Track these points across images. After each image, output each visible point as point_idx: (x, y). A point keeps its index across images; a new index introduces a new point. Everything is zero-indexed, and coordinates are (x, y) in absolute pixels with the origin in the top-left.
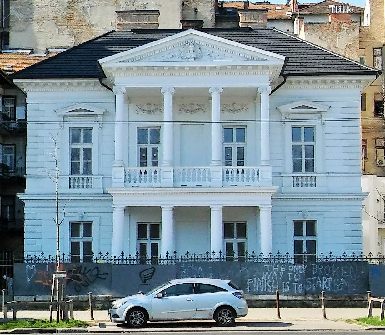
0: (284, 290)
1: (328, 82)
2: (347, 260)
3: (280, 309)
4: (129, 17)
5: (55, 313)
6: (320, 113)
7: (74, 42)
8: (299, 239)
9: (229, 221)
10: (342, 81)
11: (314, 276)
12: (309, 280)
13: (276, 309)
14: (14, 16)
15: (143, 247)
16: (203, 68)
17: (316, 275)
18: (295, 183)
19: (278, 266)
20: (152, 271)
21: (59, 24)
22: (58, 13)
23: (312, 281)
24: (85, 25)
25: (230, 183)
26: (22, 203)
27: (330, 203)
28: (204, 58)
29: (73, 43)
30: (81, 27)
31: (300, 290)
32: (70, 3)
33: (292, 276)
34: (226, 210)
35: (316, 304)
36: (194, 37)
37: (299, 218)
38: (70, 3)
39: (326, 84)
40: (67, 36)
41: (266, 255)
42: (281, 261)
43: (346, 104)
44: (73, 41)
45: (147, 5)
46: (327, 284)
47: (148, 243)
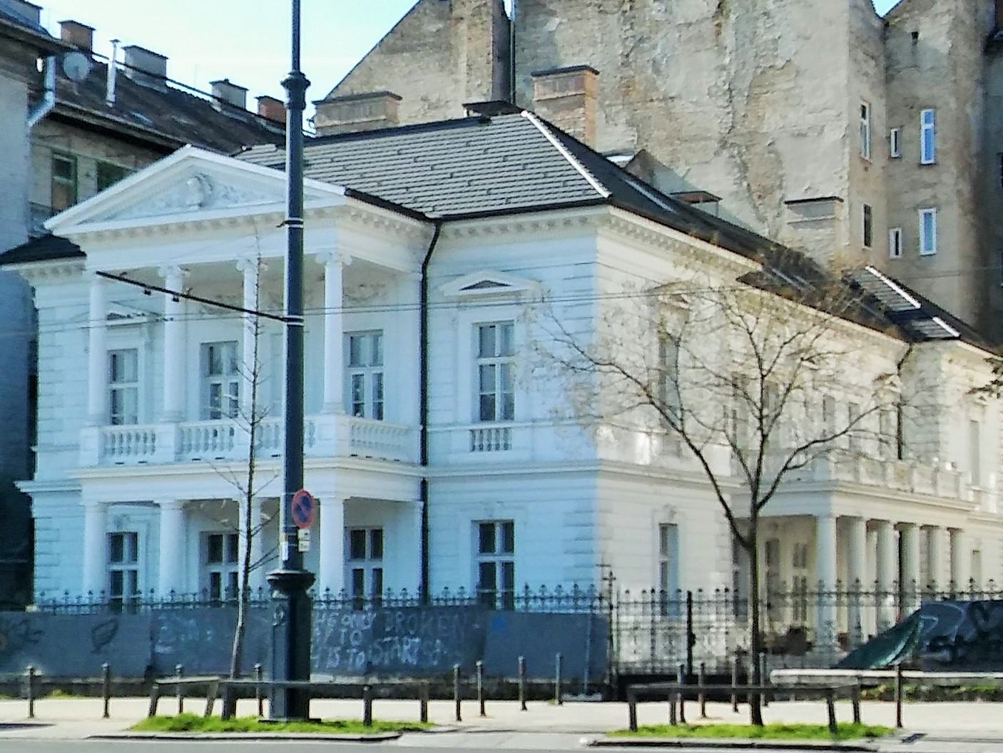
0: (330, 663)
1: (575, 222)
2: (450, 603)
3: (463, 703)
4: (335, 112)
5: (266, 703)
6: (517, 293)
7: (636, 139)
8: (488, 558)
9: (359, 524)
10: (536, 225)
11: (389, 634)
12: (380, 643)
13: (453, 704)
14: (524, 95)
15: (358, 574)
16: (216, 224)
17: (392, 634)
18: (477, 444)
19: (323, 616)
20: (111, 626)
21: (607, 102)
22: (605, 81)
23: (383, 645)
24: (657, 99)
25: (117, 458)
26: (27, 499)
27: (537, 483)
28: (220, 203)
29: (633, 141)
30: (649, 104)
31: (360, 661)
32: (627, 56)
33: (347, 634)
34: (353, 506)
35: (385, 693)
36: (191, 162)
37: (484, 517)
38: (627, 56)
39: (572, 225)
40: (622, 128)
41: (162, 594)
42: (331, 606)
43: (570, 272)
44: (633, 136)
45: (780, 41)
46: (411, 652)
47: (367, 566)
